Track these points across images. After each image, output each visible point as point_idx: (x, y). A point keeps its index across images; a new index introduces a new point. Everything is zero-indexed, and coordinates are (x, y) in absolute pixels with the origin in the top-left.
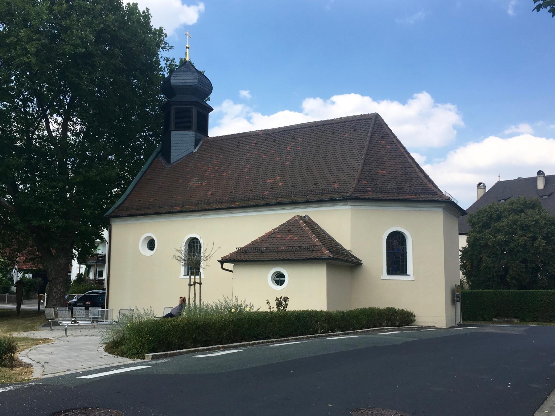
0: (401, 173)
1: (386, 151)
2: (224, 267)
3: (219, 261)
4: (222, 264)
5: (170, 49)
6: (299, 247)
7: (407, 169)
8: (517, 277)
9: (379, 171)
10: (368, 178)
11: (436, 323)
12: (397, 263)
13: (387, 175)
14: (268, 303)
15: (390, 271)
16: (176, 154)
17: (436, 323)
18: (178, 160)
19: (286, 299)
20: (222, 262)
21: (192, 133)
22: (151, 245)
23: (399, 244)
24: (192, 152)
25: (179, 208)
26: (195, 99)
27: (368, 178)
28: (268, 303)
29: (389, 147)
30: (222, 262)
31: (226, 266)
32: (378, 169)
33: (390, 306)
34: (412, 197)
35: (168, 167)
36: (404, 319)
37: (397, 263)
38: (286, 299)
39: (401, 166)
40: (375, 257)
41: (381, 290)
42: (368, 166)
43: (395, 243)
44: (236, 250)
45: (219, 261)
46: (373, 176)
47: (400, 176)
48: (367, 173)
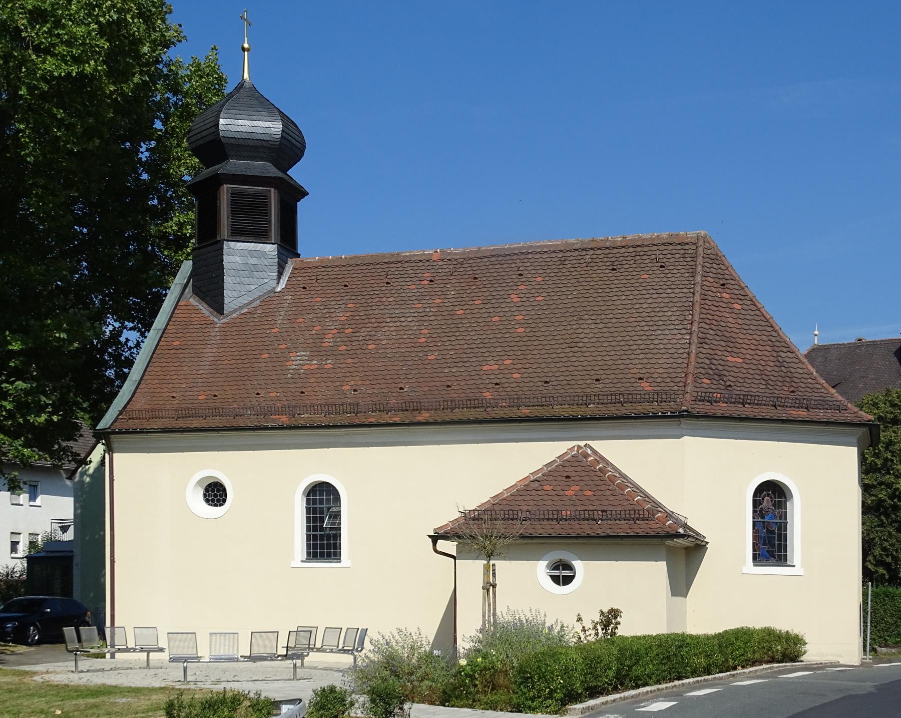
0: (772, 364)
1: (734, 316)
2: (438, 548)
3: (430, 536)
4: (435, 543)
5: (180, 41)
6: (603, 511)
7: (783, 355)
8: (889, 560)
9: (730, 358)
10: (711, 372)
11: (841, 656)
12: (771, 544)
13: (746, 366)
14: (579, 619)
15: (758, 558)
16: (238, 292)
17: (841, 656)
18: (241, 308)
19: (615, 613)
20: (435, 539)
21: (271, 249)
22: (215, 493)
23: (774, 505)
24: (273, 291)
25: (284, 420)
26: (272, 171)
27: (711, 372)
28: (579, 619)
29: (739, 307)
30: (435, 539)
31: (442, 545)
32: (726, 354)
33: (767, 626)
34: (802, 414)
35: (220, 321)
36: (782, 648)
37: (771, 544)
38: (615, 613)
39: (768, 348)
40: (728, 530)
41: (729, 595)
42: (706, 346)
43: (767, 503)
44: (458, 515)
45: (430, 536)
46: (721, 368)
47: (769, 368)
48: (708, 362)
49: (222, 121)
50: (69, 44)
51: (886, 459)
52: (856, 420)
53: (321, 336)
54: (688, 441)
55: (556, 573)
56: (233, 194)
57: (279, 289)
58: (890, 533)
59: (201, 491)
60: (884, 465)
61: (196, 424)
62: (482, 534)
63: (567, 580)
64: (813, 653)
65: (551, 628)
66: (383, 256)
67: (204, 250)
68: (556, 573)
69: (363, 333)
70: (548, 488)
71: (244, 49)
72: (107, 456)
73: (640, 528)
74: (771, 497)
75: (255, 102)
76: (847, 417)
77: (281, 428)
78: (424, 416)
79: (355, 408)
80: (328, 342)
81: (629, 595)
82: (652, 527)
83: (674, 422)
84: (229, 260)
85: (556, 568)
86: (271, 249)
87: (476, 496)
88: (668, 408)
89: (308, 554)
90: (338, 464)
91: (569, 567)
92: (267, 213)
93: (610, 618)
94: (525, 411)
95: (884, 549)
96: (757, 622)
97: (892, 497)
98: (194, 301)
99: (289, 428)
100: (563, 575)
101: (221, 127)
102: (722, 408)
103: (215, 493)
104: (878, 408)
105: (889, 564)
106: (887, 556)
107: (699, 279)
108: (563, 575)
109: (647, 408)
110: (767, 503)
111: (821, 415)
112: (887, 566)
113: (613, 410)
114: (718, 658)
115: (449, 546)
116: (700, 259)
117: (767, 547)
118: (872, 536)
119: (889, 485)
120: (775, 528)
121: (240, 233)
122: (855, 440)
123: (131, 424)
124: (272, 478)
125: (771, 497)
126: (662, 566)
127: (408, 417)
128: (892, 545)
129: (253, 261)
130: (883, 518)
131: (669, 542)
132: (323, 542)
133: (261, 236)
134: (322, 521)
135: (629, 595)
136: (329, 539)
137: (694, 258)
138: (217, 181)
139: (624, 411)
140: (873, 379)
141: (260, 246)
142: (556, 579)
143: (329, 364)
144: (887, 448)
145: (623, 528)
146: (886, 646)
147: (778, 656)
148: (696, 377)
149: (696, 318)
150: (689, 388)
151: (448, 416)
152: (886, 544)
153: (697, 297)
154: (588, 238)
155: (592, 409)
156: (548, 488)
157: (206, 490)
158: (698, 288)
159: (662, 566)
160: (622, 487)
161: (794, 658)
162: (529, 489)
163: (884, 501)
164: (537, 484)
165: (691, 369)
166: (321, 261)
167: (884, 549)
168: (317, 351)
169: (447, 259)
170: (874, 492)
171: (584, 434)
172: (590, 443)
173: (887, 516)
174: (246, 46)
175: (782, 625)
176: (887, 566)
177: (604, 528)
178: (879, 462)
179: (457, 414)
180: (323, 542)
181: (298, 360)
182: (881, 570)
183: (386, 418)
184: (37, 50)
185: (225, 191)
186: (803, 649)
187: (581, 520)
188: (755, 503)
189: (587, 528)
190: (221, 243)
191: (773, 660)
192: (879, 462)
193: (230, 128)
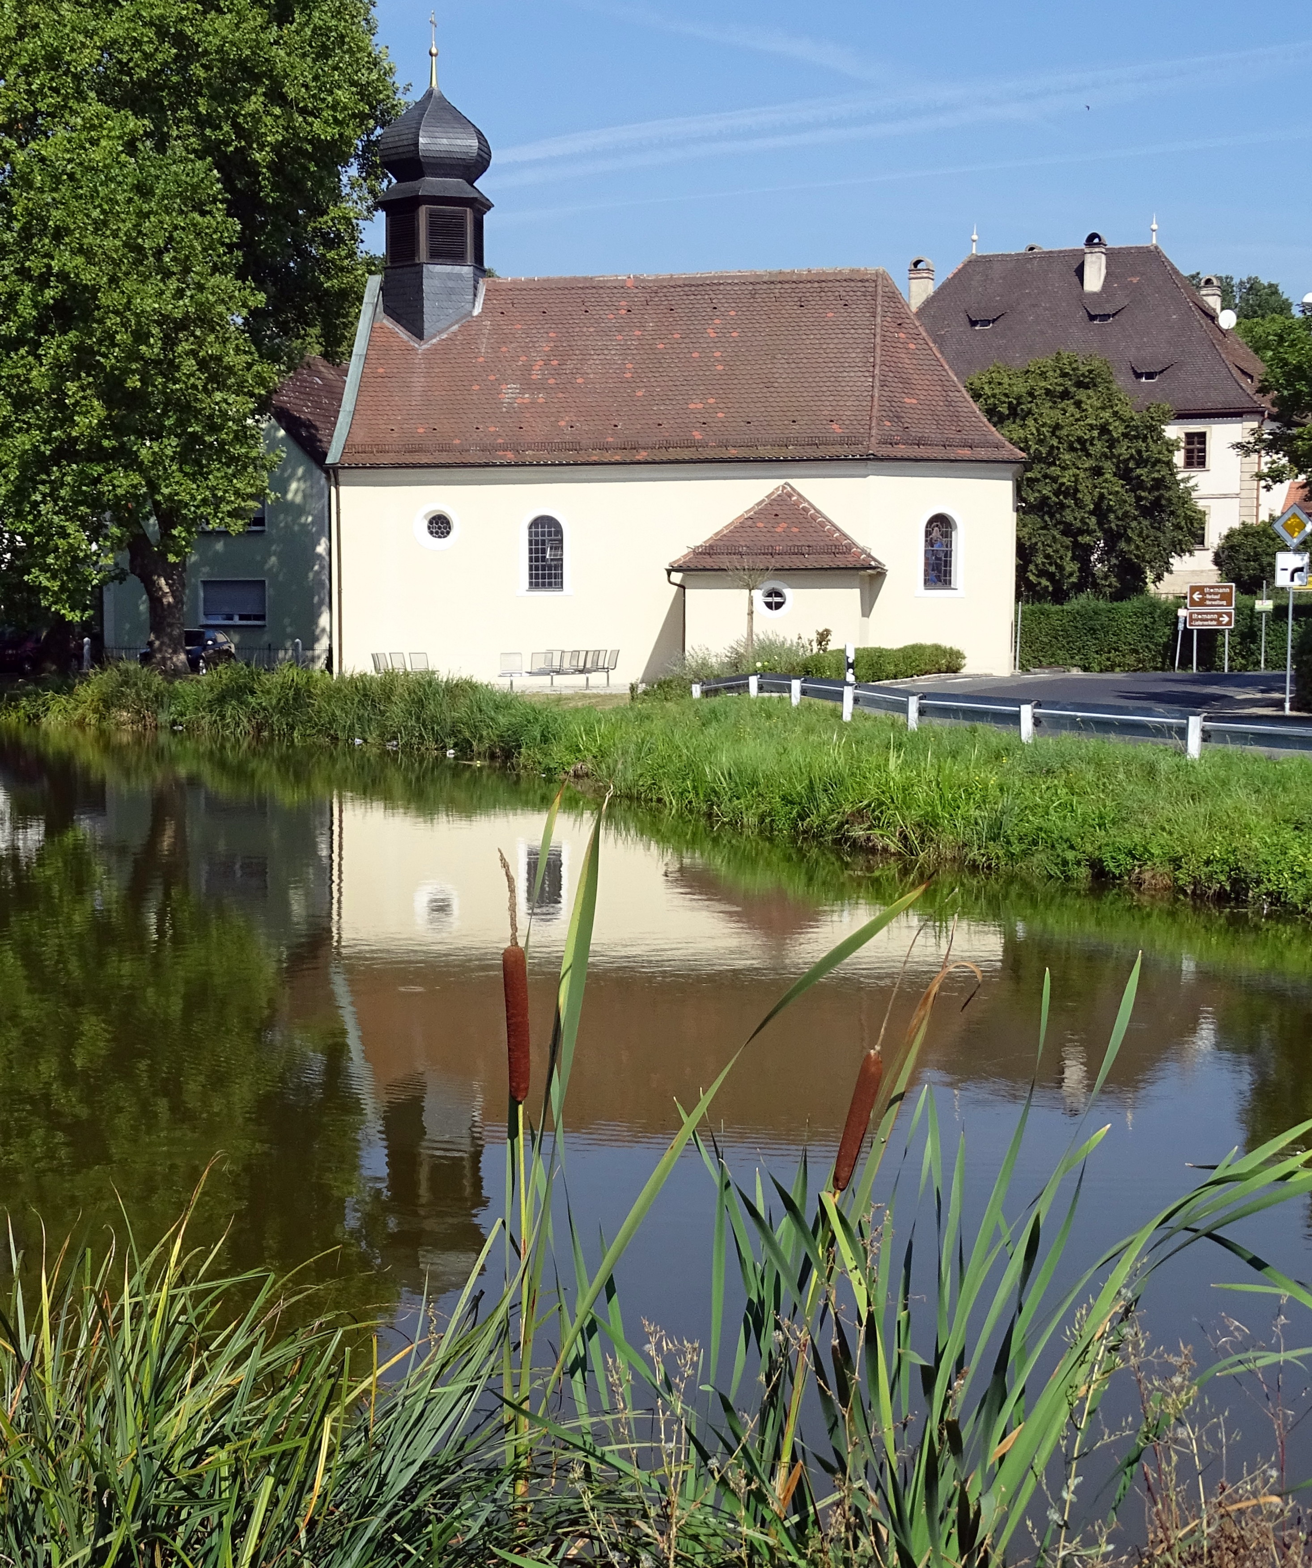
8: (1052, 569)
12: (938, 571)
20: (669, 572)
21: (466, 271)
22: (440, 525)
25: (510, 456)
34: (966, 453)
37: (938, 571)
40: (904, 560)
41: (907, 615)
43: (936, 533)
49: (421, 140)
50: (334, 108)
51: (1052, 447)
52: (1011, 458)
53: (528, 369)
54: (872, 478)
55: (769, 600)
56: (431, 215)
57: (476, 312)
58: (1054, 537)
59: (426, 523)
60: (1050, 453)
61: (424, 460)
62: (703, 567)
63: (779, 605)
64: (972, 667)
65: (783, 643)
66: (575, 279)
67: (399, 271)
68: (769, 600)
69: (570, 365)
70: (760, 525)
71: (431, 54)
72: (333, 490)
73: (840, 561)
74: (940, 526)
75: (449, 117)
76: (1003, 454)
77: (509, 465)
78: (642, 455)
79: (576, 447)
80: (536, 375)
81: (816, 616)
82: (850, 561)
83: (863, 463)
84: (428, 285)
85: (769, 595)
86: (466, 271)
87: (701, 533)
88: (858, 451)
89: (531, 583)
90: (581, 504)
91: (779, 594)
92: (463, 235)
93: (823, 637)
94: (733, 452)
95: (1048, 556)
96: (927, 639)
97: (1057, 494)
98: (388, 323)
99: (517, 465)
100: (775, 600)
101: (421, 147)
102: (902, 450)
103: (440, 525)
104: (1046, 379)
105: (1053, 574)
106: (1050, 564)
107: (879, 320)
108: (775, 600)
109: (840, 450)
110: (936, 533)
111: (982, 453)
112: (1051, 577)
113: (811, 452)
114: (902, 667)
115: (677, 577)
116: (879, 299)
117: (935, 573)
118: (1034, 540)
119: (1054, 480)
120: (942, 555)
121: (438, 255)
122: (1010, 475)
123: (360, 459)
124: (496, 512)
125: (940, 526)
126: (857, 592)
127: (628, 456)
128: (1056, 551)
129: (450, 284)
130: (1047, 518)
131: (862, 573)
132: (546, 571)
133: (457, 257)
134: (544, 551)
135: (816, 616)
136: (550, 569)
137: (874, 298)
138: (415, 202)
139: (819, 454)
140: (1046, 309)
141: (457, 269)
142: (769, 605)
143: (541, 398)
144: (1053, 433)
145: (826, 561)
146: (1040, 667)
147: (944, 668)
148: (880, 420)
149: (878, 361)
150: (874, 432)
151: (664, 455)
152: (1050, 551)
153: (878, 339)
154: (775, 269)
155: (791, 451)
156: (760, 525)
157: (431, 522)
158: (878, 330)
159: (857, 592)
160: (823, 525)
161: (954, 669)
162: (745, 525)
163: (1049, 498)
164: (750, 522)
165: (875, 413)
166: (514, 282)
167: (1048, 556)
168: (528, 385)
169: (641, 285)
170: (1037, 487)
171: (784, 473)
172: (790, 481)
173: (1052, 516)
174: (434, 51)
175: (947, 643)
176: (1051, 577)
177: (810, 561)
178: (1044, 451)
179: (673, 454)
180: (546, 571)
181: (509, 392)
182: (1045, 582)
183: (608, 456)
184: (303, 111)
185: (423, 211)
186: (963, 662)
187: (787, 553)
188: (928, 533)
189: (797, 562)
190: (421, 265)
191: (940, 671)
192: (1044, 451)
193: (433, 148)
